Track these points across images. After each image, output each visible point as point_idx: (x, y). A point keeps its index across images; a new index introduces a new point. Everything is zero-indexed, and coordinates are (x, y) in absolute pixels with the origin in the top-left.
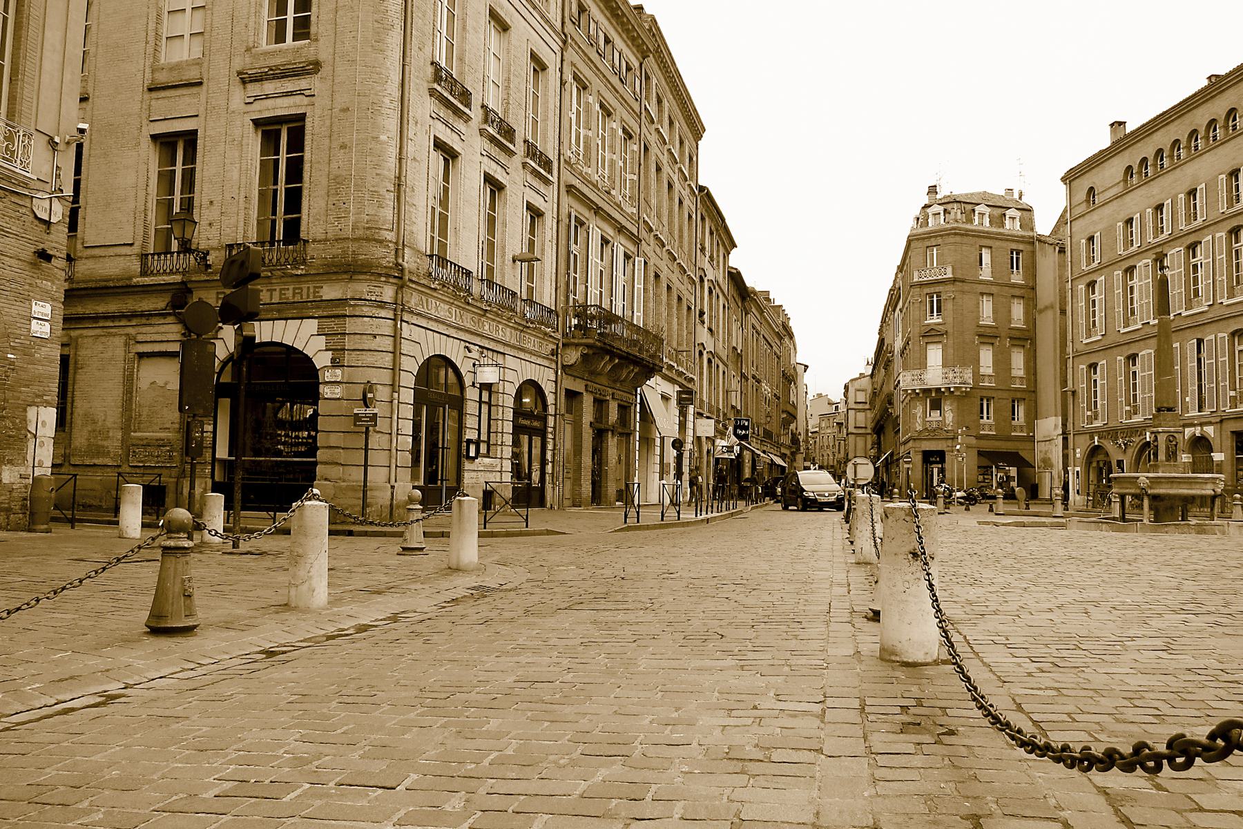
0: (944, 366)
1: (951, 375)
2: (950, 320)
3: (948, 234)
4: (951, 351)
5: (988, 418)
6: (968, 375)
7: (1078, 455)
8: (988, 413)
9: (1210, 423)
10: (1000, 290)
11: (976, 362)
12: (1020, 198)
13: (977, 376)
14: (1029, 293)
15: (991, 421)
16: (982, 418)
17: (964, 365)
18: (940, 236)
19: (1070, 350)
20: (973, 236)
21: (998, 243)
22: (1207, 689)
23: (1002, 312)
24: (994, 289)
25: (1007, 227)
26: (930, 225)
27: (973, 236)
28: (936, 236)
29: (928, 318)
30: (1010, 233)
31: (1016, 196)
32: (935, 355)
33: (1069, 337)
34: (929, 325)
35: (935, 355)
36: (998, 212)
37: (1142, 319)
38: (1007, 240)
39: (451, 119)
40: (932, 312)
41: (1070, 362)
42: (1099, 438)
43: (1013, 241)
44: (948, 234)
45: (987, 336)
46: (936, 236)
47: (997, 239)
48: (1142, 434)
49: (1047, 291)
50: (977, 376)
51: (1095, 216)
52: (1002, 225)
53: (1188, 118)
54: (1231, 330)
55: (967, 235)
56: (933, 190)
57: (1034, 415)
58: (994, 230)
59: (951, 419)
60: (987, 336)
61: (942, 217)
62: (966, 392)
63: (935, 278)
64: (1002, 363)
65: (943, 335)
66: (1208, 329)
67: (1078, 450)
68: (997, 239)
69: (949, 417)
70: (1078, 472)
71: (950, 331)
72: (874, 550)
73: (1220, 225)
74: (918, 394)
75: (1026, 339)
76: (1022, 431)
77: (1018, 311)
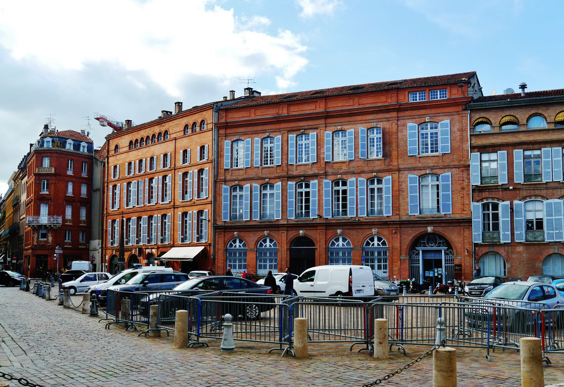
0: (49, 214)
1: (52, 219)
2: (52, 193)
3: (54, 153)
4: (52, 208)
5: (68, 239)
6: (60, 220)
7: (107, 258)
8: (68, 237)
9: (154, 248)
10: (77, 181)
11: (63, 214)
12: (88, 136)
13: (64, 220)
14: (89, 181)
15: (70, 241)
16: (66, 239)
17: (58, 215)
18: (49, 153)
19: (105, 212)
20: (65, 154)
21: (77, 158)
22: (169, 381)
23: (77, 190)
24: (74, 179)
25: (81, 150)
26: (45, 146)
27: (65, 154)
28: (48, 153)
29: (42, 191)
30: (81, 154)
31: (86, 134)
32: (44, 210)
33: (105, 207)
34: (42, 194)
35: (44, 210)
36: (77, 143)
37: (133, 204)
38: (81, 157)
39: (232, 351)
40: (44, 188)
41: (105, 217)
42: (116, 252)
43: (84, 157)
44: (54, 153)
45: (69, 201)
46: (48, 153)
47: (76, 156)
48: (131, 250)
49: (97, 182)
50: (64, 220)
51: (118, 157)
52: (79, 149)
53: (152, 129)
54: (262, 137)
55: (62, 154)
56: (46, 127)
57: (89, 238)
58: (75, 152)
59: (51, 240)
60: (69, 201)
61: (51, 144)
62: (59, 227)
63: (46, 172)
64: (76, 214)
65: (49, 200)
66: (155, 212)
67: (107, 256)
68: (76, 156)
69: (50, 239)
70: (440, 316)
71: (53, 198)
72: (369, 135)
73: (161, 173)
74: (35, 227)
75: (87, 203)
76: (84, 246)
77: (84, 190)
